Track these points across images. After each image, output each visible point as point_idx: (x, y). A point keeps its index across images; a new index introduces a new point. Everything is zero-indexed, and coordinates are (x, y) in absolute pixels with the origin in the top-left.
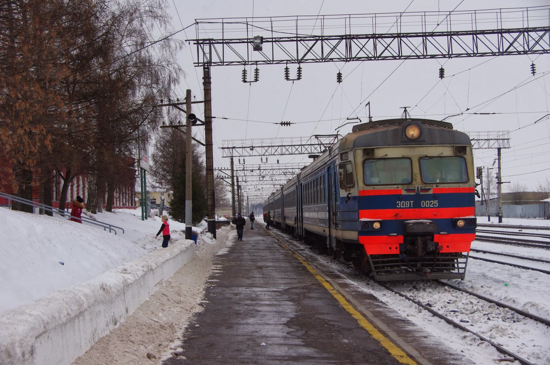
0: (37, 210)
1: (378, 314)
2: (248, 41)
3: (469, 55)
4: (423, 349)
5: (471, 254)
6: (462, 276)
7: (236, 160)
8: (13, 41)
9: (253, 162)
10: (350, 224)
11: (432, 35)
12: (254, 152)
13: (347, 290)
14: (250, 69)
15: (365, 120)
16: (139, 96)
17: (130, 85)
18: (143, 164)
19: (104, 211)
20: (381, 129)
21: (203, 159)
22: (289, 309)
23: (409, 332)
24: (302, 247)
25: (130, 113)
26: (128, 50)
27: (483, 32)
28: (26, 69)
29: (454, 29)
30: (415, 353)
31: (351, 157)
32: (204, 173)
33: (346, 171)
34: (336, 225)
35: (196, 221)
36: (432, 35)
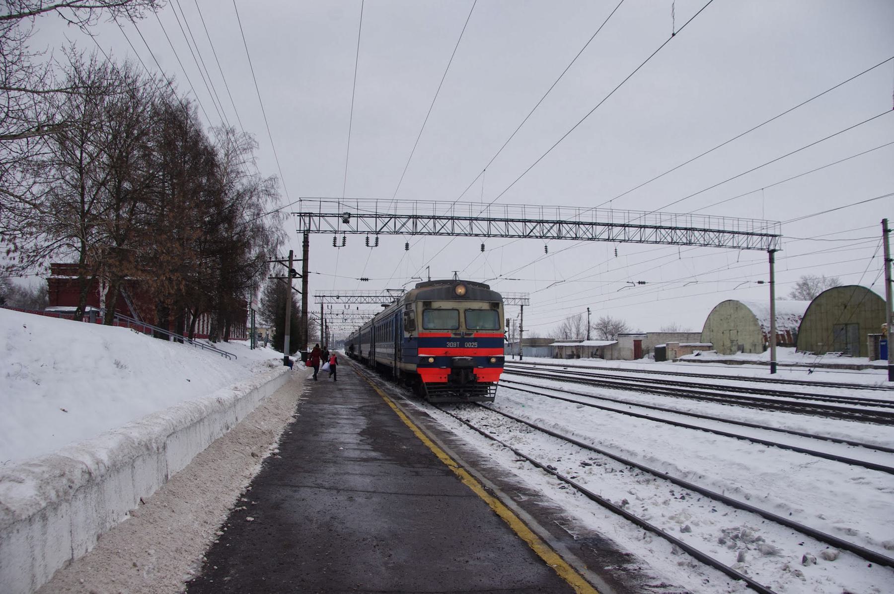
0: (172, 338)
1: (429, 428)
2: (339, 216)
3: (502, 236)
4: (462, 453)
5: (500, 383)
6: (492, 399)
7: (325, 306)
8: (163, 210)
9: (338, 308)
10: (411, 358)
11: (477, 219)
12: (340, 300)
13: (406, 408)
14: (340, 237)
15: (426, 280)
16: (253, 253)
17: (247, 245)
18: (254, 306)
19: (222, 341)
20: (438, 287)
21: (300, 304)
22: (362, 422)
23: (453, 441)
24: (374, 375)
25: (247, 266)
26: (247, 218)
27: (512, 221)
28: (170, 231)
29: (492, 216)
30: (456, 457)
31: (413, 307)
32: (300, 315)
33: (409, 318)
34: (401, 359)
35: (292, 352)
36: (477, 219)
